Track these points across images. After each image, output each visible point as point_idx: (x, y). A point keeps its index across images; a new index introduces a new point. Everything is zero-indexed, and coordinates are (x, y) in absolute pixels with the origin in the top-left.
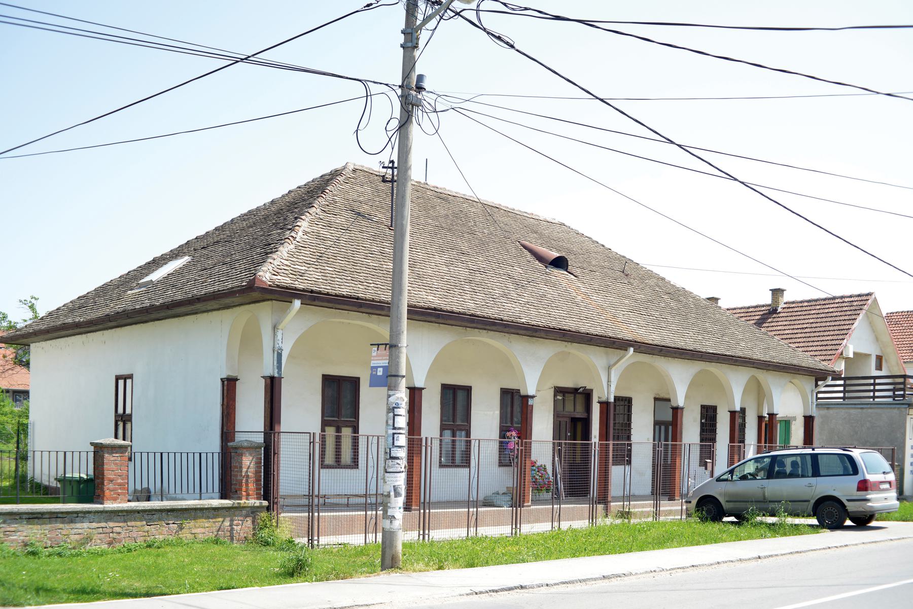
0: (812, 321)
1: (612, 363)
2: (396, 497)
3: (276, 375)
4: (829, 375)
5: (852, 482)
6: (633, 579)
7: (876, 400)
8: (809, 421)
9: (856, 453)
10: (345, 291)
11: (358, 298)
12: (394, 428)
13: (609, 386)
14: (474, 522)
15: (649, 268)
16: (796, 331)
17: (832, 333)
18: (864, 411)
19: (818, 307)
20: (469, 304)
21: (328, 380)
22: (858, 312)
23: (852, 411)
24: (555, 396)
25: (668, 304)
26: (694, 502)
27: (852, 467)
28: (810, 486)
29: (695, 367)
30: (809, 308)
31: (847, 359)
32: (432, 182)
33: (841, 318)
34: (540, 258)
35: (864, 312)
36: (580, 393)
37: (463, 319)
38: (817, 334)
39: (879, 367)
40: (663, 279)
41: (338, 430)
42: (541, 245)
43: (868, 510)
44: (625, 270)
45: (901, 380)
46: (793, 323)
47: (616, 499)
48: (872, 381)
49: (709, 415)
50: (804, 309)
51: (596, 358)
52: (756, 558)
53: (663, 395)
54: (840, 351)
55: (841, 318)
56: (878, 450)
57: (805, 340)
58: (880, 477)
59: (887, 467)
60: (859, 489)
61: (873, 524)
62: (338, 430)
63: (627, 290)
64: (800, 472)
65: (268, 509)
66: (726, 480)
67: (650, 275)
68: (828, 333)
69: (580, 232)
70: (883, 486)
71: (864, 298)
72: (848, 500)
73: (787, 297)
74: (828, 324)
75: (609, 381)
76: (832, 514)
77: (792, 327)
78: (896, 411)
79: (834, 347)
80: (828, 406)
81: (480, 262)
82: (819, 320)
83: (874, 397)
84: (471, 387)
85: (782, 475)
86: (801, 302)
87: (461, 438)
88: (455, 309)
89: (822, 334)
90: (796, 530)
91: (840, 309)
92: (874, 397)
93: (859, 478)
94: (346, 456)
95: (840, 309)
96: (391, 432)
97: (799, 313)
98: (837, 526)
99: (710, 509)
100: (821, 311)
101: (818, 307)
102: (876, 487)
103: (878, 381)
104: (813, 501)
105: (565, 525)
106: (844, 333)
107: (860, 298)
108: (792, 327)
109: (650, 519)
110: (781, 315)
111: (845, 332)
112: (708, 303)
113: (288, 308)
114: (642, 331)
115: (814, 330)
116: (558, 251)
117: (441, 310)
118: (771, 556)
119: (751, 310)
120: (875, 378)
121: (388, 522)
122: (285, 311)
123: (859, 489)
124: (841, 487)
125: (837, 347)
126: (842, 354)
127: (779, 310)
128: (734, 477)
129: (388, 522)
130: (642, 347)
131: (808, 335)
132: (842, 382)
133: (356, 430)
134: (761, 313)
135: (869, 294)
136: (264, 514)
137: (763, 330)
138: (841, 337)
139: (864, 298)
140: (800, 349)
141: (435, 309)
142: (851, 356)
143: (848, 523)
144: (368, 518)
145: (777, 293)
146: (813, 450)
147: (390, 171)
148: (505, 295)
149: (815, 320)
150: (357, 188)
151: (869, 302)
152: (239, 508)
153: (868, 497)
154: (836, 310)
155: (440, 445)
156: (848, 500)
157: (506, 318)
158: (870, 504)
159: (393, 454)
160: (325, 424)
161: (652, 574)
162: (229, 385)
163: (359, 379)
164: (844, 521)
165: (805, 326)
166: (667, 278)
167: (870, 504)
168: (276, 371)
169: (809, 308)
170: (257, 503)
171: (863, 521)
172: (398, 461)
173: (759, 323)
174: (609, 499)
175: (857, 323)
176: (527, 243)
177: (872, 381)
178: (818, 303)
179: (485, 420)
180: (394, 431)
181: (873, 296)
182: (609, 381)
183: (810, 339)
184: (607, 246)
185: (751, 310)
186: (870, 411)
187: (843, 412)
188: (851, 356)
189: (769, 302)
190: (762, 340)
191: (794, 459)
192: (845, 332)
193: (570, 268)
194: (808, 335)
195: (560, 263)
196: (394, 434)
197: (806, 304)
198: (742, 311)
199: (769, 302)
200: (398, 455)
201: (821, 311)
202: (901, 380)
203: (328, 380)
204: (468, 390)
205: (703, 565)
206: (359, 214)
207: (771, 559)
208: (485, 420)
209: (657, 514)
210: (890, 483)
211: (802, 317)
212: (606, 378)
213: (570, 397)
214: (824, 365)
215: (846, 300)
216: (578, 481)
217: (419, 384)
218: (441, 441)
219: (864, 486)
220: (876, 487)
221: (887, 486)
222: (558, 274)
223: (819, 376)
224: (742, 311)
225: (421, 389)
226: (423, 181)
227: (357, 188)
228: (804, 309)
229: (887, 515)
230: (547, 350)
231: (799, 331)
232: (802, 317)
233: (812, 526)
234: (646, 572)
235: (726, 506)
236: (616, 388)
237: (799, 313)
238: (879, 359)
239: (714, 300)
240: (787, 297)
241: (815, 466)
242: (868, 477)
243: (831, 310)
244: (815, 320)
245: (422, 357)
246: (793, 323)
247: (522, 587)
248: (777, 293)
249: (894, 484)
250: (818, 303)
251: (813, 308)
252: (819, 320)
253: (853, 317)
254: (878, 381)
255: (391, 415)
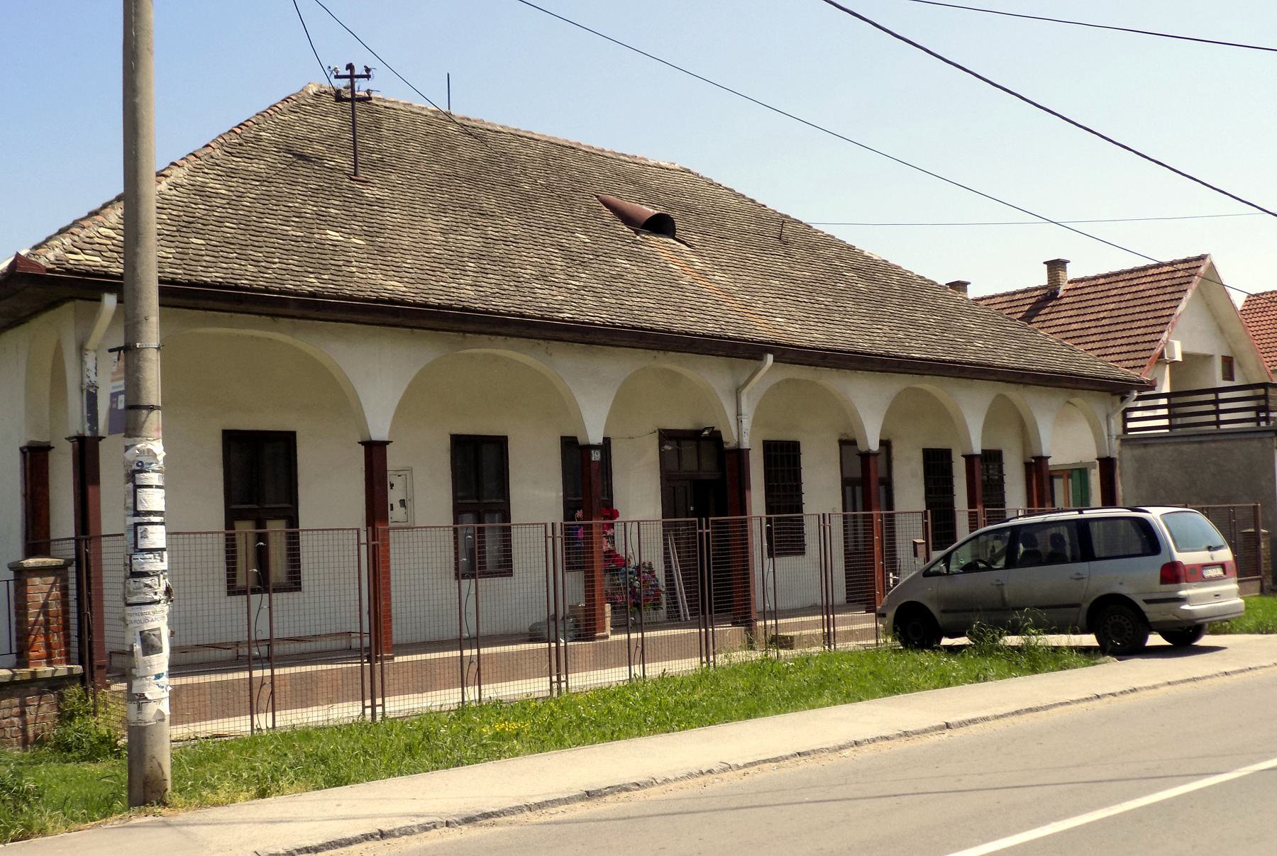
0: (1112, 306)
1: (742, 382)
2: (146, 653)
3: (88, 433)
4: (1133, 388)
5: (1149, 568)
6: (655, 793)
7: (1222, 427)
8: (1107, 465)
9: (1155, 515)
10: (214, 276)
11: (237, 287)
12: (137, 513)
13: (739, 422)
14: (558, 666)
15: (828, 230)
16: (1087, 325)
17: (1144, 323)
18: (1205, 446)
19: (1121, 284)
20: (465, 291)
21: (234, 440)
22: (1184, 287)
23: (1185, 448)
24: (661, 445)
25: (851, 286)
26: (891, 614)
27: (1149, 540)
28: (1079, 578)
29: (895, 384)
30: (1107, 287)
31: (1173, 364)
32: (458, 111)
33: (1158, 299)
34: (627, 218)
35: (1194, 286)
36: (706, 438)
37: (446, 317)
38: (1121, 327)
39: (1228, 374)
40: (851, 248)
41: (260, 524)
42: (639, 201)
43: (1184, 617)
44: (783, 234)
45: (1261, 392)
46: (1082, 312)
47: (765, 615)
48: (1212, 397)
49: (936, 465)
50: (1100, 288)
51: (712, 377)
52: (940, 728)
53: (851, 436)
54: (1158, 351)
55: (1158, 299)
56: (1201, 510)
57: (1101, 337)
58: (1201, 557)
59: (1219, 538)
60: (1164, 580)
61: (1205, 640)
62: (260, 524)
63: (780, 264)
64: (1068, 553)
65: (82, 679)
66: (938, 574)
67: (830, 241)
68: (1138, 324)
69: (716, 180)
70: (1210, 573)
71: (1194, 264)
72: (1148, 602)
73: (1072, 272)
74: (1138, 309)
75: (738, 414)
76: (1122, 629)
77: (1081, 319)
78: (1256, 444)
79: (1147, 346)
80: (1144, 441)
81: (512, 226)
82: (1123, 305)
83: (1218, 423)
84: (506, 438)
85: (1034, 559)
86: (1095, 278)
87: (491, 525)
88: (432, 300)
89: (1128, 326)
90: (1056, 659)
91: (1155, 285)
92: (1218, 423)
93: (1160, 560)
94: (278, 568)
95: (1155, 285)
96: (132, 520)
97: (1092, 296)
98: (1132, 648)
99: (917, 628)
100: (1126, 290)
101: (1121, 284)
102: (1196, 574)
103: (1222, 396)
104: (1086, 606)
105: (654, 669)
106: (1163, 321)
107: (1186, 265)
108: (1081, 319)
109: (816, 649)
110: (1067, 300)
111: (1165, 320)
112: (950, 292)
113: (99, 307)
114: (794, 328)
115: (1116, 320)
116: (654, 208)
117: (403, 302)
118: (973, 721)
119: (1018, 296)
120: (1217, 391)
121: (134, 706)
122: (93, 315)
123: (1164, 580)
124: (1132, 578)
125: (1152, 345)
126: (1162, 355)
127: (1061, 293)
128: (953, 568)
129: (134, 706)
130: (789, 354)
131: (1106, 329)
132: (1164, 401)
133: (293, 521)
134: (1033, 300)
135: (1202, 258)
136: (76, 689)
137: (1035, 326)
138: (1159, 329)
139: (1194, 264)
140: (1081, 348)
141: (391, 301)
142: (1179, 358)
143: (1155, 640)
144: (256, 685)
145: (1056, 266)
146: (1081, 512)
147: (346, 82)
148: (543, 277)
149: (1117, 305)
150: (311, 119)
151: (1202, 270)
152: (34, 678)
153: (1183, 593)
154: (1149, 286)
155: (456, 538)
156: (1148, 602)
157: (528, 312)
158: (1186, 607)
159: (136, 568)
160: (231, 517)
161: (701, 779)
162: (36, 459)
163: (293, 434)
164: (1145, 639)
165: (1101, 315)
166: (858, 246)
167: (1186, 607)
168: (87, 425)
169: (1107, 287)
170: (62, 669)
171: (1184, 638)
172: (148, 581)
173: (1028, 317)
174: (754, 617)
175: (1182, 306)
176: (612, 198)
177: (1212, 397)
178: (1121, 277)
179: (536, 496)
180: (137, 520)
181: (1208, 261)
182: (738, 414)
183: (1110, 336)
184: (759, 201)
185: (1018, 296)
186: (1213, 445)
187: (1169, 450)
188: (1179, 358)
189: (1044, 282)
190: (1016, 336)
191: (1054, 530)
192: (1165, 320)
193: (679, 233)
194: (1106, 329)
195: (661, 225)
196: (136, 525)
197: (1102, 281)
198: (1005, 298)
199: (1044, 282)
200: (147, 568)
201: (1126, 290)
202: (1261, 392)
203: (234, 440)
204: (500, 443)
205: (821, 750)
206: (301, 157)
207: (972, 727)
208: (536, 496)
209: (828, 638)
210: (1222, 565)
211: (1097, 302)
212: (743, 412)
213: (688, 447)
214: (1121, 372)
215: (1166, 269)
216: (715, 589)
217: (378, 434)
218: (455, 530)
219: (1173, 573)
220: (1196, 574)
221: (1219, 572)
222: (657, 242)
223: (1118, 389)
224: (1005, 298)
225: (383, 444)
226: (445, 109)
227: (311, 119)
228: (1100, 288)
229: (1223, 624)
230: (619, 367)
231: (1093, 324)
232: (1097, 302)
233: (1086, 650)
234: (690, 775)
235: (942, 619)
236: (755, 423)
237: (1092, 296)
238: (1228, 363)
239: (960, 286)
240: (1072, 272)
241: (1083, 544)
242: (1180, 557)
243: (1141, 287)
244: (1117, 305)
245: (381, 383)
246: (1082, 312)
247: (383, 835)
248: (1056, 266)
249: (1232, 568)
250: (1121, 277)
251: (1114, 285)
252: (1123, 305)
253: (1177, 296)
254: (1222, 396)
255: (131, 485)
